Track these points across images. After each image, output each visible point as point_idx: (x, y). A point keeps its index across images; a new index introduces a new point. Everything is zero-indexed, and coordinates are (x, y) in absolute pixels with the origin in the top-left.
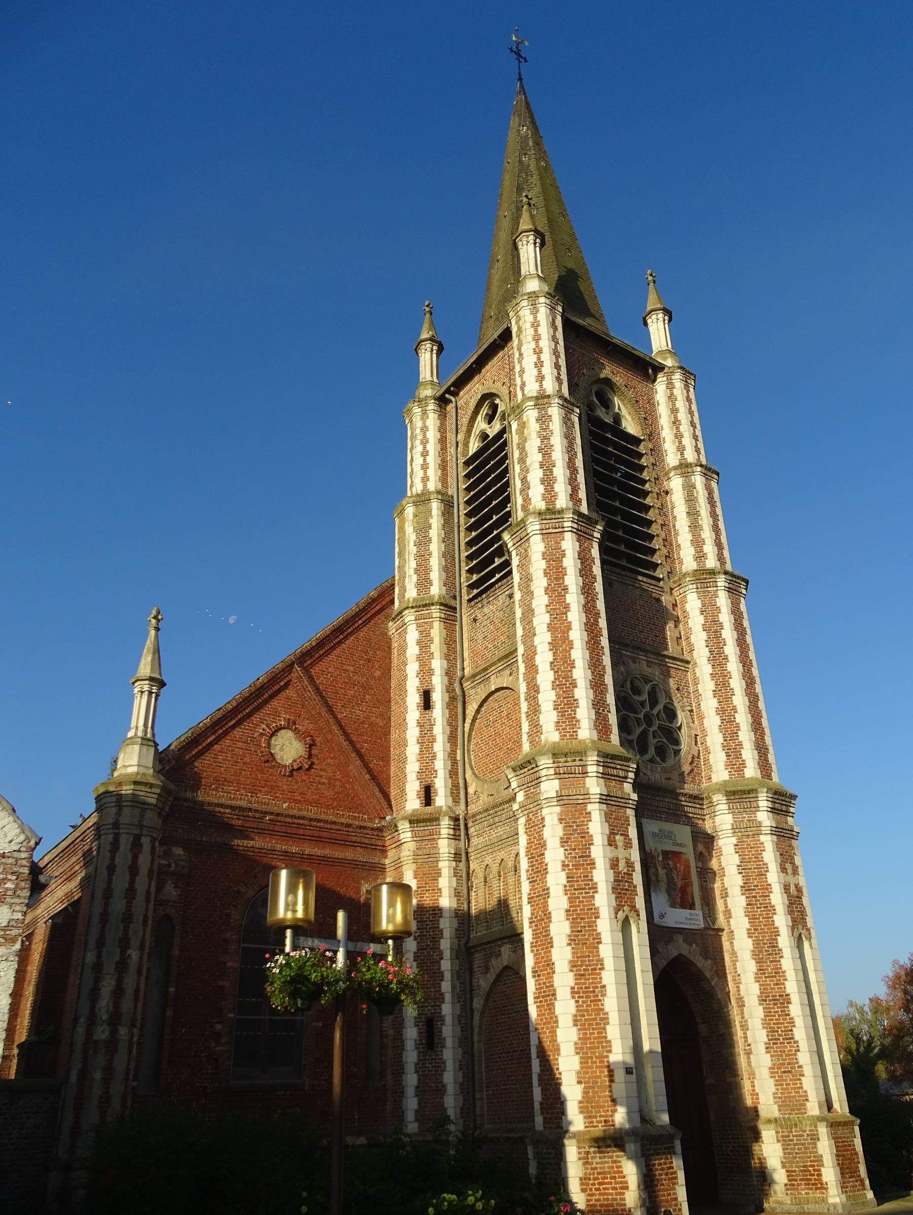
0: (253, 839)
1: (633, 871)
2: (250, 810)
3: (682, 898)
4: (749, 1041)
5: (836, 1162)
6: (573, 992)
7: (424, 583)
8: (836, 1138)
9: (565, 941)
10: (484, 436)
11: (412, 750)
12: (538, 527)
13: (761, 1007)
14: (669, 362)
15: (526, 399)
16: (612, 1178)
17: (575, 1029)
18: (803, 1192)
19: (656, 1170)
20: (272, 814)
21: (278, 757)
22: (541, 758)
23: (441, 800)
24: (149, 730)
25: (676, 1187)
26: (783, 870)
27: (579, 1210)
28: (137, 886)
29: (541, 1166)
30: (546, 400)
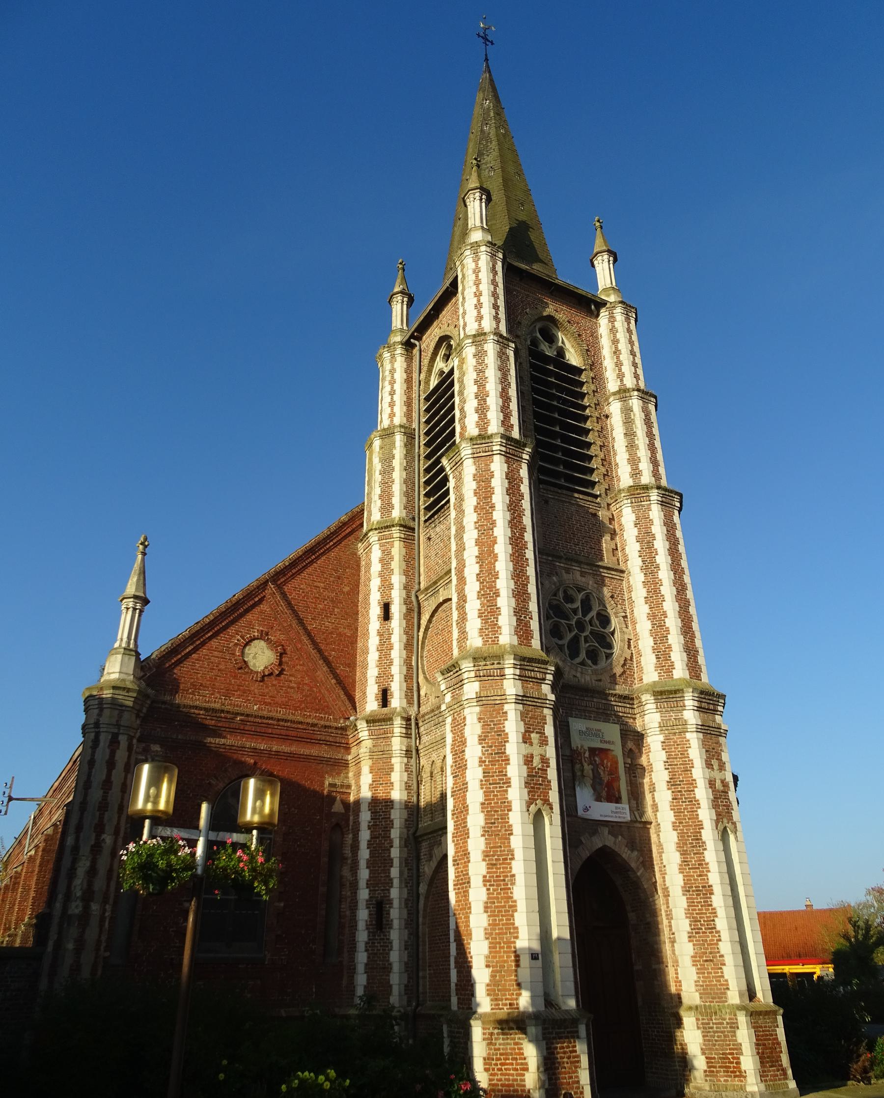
0: (225, 737)
1: (548, 767)
2: (222, 711)
3: (608, 792)
4: (674, 930)
5: (755, 1051)
6: (485, 881)
7: (387, 507)
8: (756, 1027)
9: (479, 832)
10: (442, 372)
11: (373, 657)
12: (470, 452)
13: (685, 897)
14: (612, 298)
15: (467, 337)
16: (513, 1059)
17: (485, 915)
18: (722, 1079)
19: (558, 1053)
20: (242, 715)
21: (251, 664)
22: (463, 661)
23: (396, 701)
24: (132, 642)
25: (579, 1070)
26: (709, 765)
27: (482, 1089)
28: (113, 778)
29: (453, 1045)
30: (482, 337)
